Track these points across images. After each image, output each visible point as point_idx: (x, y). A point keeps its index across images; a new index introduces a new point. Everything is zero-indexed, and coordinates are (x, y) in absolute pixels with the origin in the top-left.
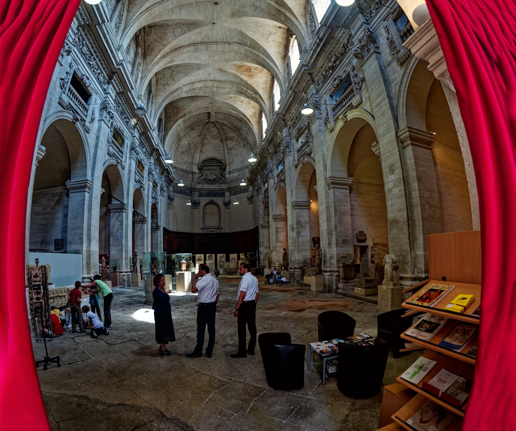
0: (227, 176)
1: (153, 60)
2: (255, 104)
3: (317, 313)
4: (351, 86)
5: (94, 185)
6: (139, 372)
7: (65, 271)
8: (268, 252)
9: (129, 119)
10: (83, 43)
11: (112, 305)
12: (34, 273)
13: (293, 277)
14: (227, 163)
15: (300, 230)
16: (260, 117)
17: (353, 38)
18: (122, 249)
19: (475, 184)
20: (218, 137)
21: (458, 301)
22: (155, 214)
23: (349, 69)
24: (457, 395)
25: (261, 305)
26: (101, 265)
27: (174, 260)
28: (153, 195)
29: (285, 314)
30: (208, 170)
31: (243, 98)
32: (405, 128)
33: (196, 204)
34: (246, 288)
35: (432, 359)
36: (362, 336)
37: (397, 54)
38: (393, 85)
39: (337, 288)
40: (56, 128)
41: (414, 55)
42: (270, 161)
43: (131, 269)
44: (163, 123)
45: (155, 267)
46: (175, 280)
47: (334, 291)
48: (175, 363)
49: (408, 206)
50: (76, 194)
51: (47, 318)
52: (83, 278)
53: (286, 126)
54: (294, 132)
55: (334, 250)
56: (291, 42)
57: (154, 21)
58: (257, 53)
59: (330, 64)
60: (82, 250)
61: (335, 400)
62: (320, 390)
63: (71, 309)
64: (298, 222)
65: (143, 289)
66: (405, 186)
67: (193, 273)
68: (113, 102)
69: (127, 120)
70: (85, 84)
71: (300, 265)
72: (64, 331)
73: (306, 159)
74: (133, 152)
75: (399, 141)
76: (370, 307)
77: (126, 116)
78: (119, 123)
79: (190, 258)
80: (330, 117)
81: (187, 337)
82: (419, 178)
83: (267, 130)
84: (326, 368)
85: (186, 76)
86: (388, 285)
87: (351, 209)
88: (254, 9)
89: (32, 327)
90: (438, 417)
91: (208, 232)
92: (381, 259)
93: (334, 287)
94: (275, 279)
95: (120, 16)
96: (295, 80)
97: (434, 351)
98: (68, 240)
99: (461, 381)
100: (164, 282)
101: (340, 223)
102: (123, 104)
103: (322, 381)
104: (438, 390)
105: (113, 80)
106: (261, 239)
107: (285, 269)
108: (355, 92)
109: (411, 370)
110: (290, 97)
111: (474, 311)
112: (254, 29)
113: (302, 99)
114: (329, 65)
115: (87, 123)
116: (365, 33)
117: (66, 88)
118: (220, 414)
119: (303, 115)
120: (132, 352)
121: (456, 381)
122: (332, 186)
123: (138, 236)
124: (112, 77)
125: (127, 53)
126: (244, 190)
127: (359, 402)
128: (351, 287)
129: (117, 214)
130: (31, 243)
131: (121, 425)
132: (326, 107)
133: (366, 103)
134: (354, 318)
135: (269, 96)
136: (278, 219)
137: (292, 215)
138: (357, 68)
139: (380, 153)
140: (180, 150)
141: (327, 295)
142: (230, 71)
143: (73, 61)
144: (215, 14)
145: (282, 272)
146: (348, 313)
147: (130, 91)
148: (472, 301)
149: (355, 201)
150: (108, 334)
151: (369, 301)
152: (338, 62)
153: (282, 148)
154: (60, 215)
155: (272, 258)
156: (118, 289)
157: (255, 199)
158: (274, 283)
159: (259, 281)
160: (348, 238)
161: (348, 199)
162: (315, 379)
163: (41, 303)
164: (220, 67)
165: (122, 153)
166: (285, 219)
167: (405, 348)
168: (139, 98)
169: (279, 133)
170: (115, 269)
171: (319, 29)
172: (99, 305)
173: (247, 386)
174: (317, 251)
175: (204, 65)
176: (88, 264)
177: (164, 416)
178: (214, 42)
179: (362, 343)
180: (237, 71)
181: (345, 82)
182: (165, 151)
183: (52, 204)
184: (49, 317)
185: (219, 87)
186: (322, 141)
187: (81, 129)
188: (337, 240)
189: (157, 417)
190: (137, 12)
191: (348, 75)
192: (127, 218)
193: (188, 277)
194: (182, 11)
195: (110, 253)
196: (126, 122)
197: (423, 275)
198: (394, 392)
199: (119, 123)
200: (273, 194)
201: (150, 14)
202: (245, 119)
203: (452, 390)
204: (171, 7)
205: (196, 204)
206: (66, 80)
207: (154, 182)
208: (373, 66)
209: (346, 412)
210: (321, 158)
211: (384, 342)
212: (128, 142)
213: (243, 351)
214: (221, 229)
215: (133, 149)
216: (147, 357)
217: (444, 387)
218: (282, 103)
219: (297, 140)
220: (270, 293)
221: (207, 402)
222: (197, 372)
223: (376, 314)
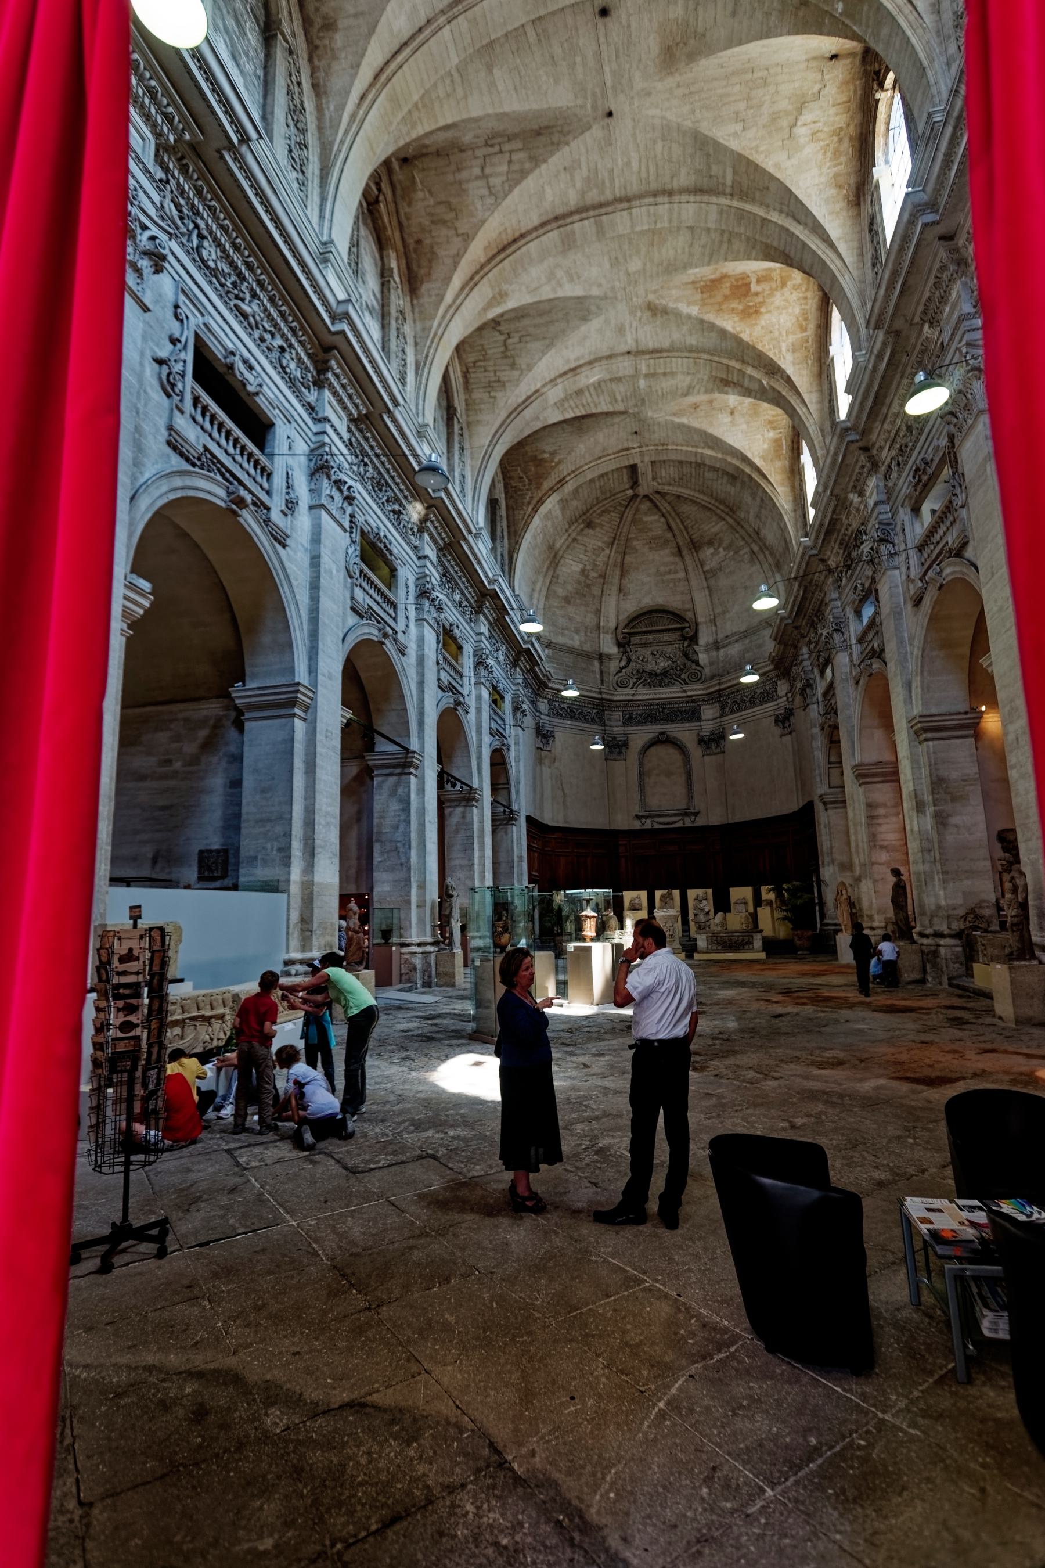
0: (703, 658)
1: (441, 298)
2: (770, 411)
5: (320, 700)
6: (438, 1274)
7: (222, 943)
9: (401, 504)
10: (197, 226)
11: (371, 1044)
12: (120, 948)
14: (700, 620)
16: (796, 452)
18: (408, 881)
20: (666, 542)
22: (503, 780)
26: (344, 923)
27: (560, 910)
28: (494, 725)
29: (877, 1088)
30: (646, 645)
31: (733, 399)
33: (619, 747)
40: (178, 527)
42: (835, 595)
43: (434, 935)
44: (503, 511)
45: (505, 930)
46: (565, 967)
48: (557, 1241)
50: (265, 722)
51: (151, 1086)
52: (288, 963)
53: (875, 466)
54: (904, 483)
56: (882, 108)
57: (414, 135)
58: (761, 212)
60: (288, 881)
63: (239, 1057)
64: (938, 784)
65: (467, 993)
67: (617, 948)
68: (345, 451)
69: (396, 507)
70: (244, 385)
71: (956, 926)
72: (206, 1128)
73: (951, 570)
74: (427, 603)
77: (390, 493)
78: (374, 516)
79: (607, 902)
81: (601, 1151)
85: (549, 347)
89: (87, 1120)
91: (656, 826)
95: (296, 111)
98: (243, 853)
100: (533, 974)
102: (377, 456)
105: (330, 375)
106: (824, 841)
110: (880, 356)
115: (275, 516)
117: (181, 395)
118: (708, 1480)
120: (422, 1197)
123: (456, 842)
124: (326, 362)
125: (356, 272)
129: (392, 780)
130: (114, 860)
131: (340, 1504)
135: (816, 369)
140: (561, 592)
142: (685, 309)
143: (182, 297)
144: (607, 69)
147: (389, 411)
150: (351, 1136)
153: (866, 548)
154: (217, 781)
155: (859, 899)
156: (392, 994)
157: (796, 720)
163: (138, 1039)
164: (651, 297)
165: (394, 606)
166: (892, 774)
168: (420, 435)
169: (855, 498)
170: (386, 934)
172: (333, 1042)
173: (681, 1316)
175: (601, 298)
176: (306, 921)
177: (503, 1465)
178: (620, 200)
180: (703, 303)
182: (517, 597)
183: (190, 748)
184: (158, 1084)
187: (259, 532)
189: (479, 1470)
190: (348, 93)
192: (421, 791)
193: (601, 959)
194: (496, 71)
195: (372, 889)
196: (394, 512)
199: (374, 516)
200: (850, 702)
201: (395, 101)
202: (748, 470)
204: (455, 61)
205: (619, 747)
206: (178, 367)
207: (494, 688)
212: (407, 575)
214: (696, 814)
215: (423, 593)
216: (469, 1217)
219: (916, 510)
220: (845, 1013)
221: (662, 1415)
222: (630, 1281)
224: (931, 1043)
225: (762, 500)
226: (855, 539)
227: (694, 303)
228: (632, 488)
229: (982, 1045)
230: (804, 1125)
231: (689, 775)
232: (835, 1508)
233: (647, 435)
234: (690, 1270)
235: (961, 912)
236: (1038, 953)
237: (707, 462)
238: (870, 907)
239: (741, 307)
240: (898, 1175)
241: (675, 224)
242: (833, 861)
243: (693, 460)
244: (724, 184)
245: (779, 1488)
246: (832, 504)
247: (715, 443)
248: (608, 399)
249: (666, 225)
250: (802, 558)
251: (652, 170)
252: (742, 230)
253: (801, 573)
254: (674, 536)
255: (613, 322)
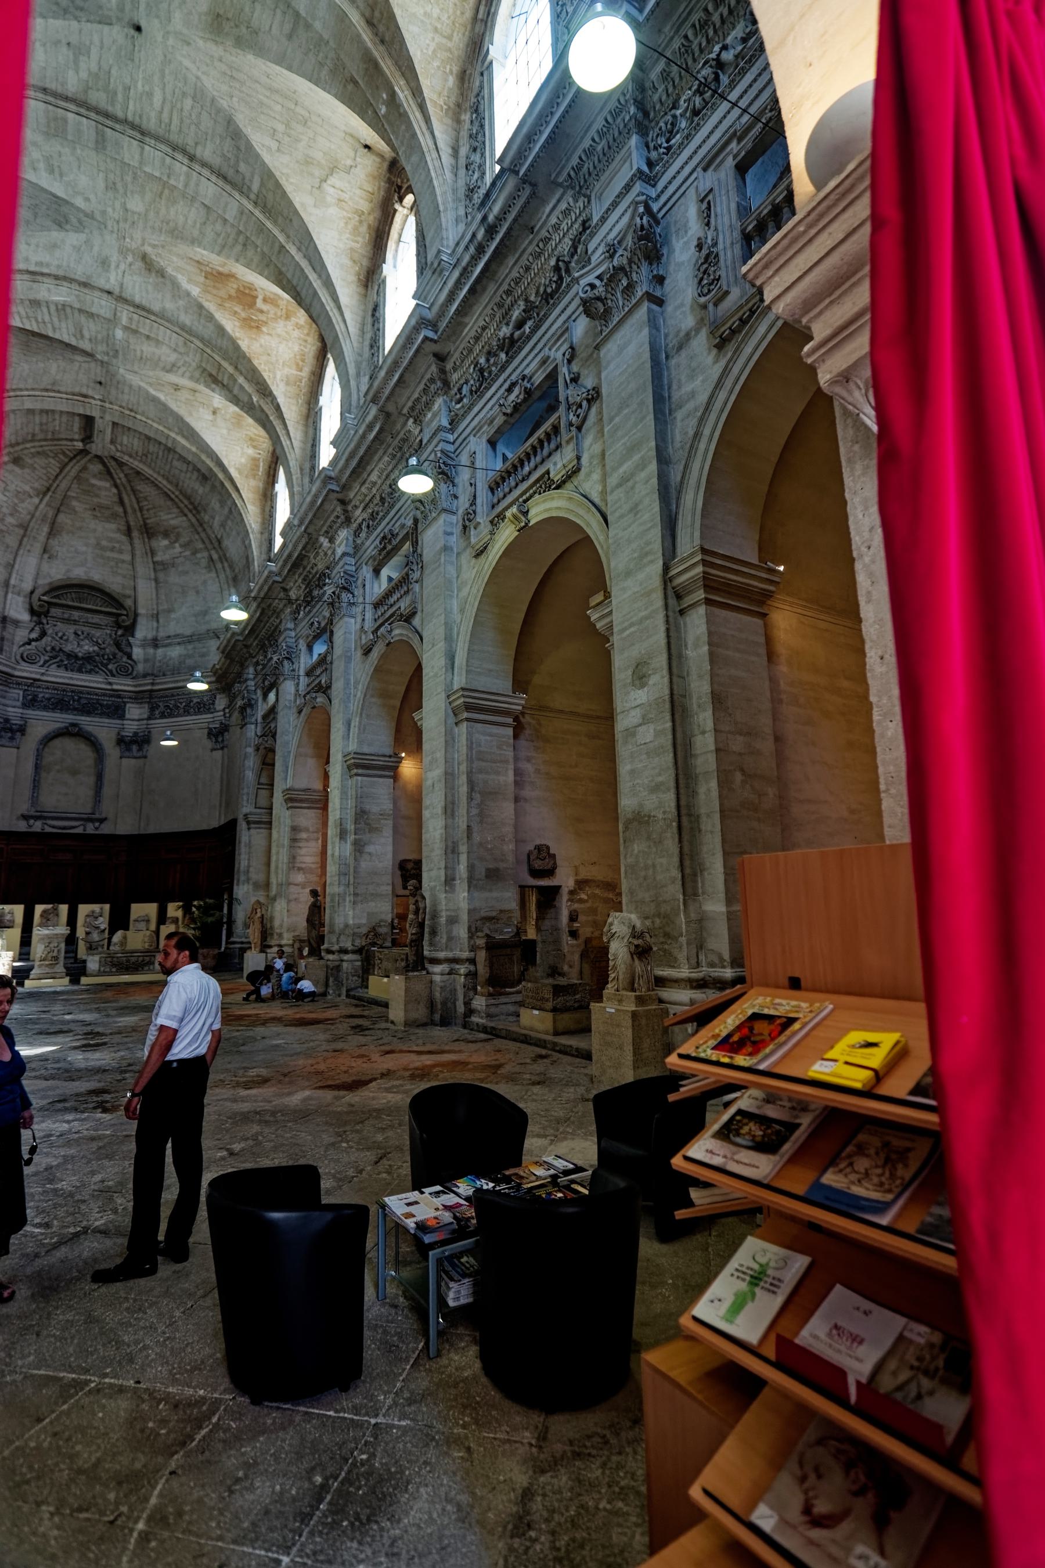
0: (137, 652)
2: (252, 428)
3: (406, 1092)
4: (556, 415)
8: (262, 900)
13: (336, 979)
15: (366, 837)
16: (271, 479)
17: (592, 235)
19: (898, 709)
21: (851, 1053)
23: (557, 354)
24: (919, 1397)
25: (227, 1071)
29: (305, 1100)
31: (218, 400)
32: (692, 554)
34: (179, 1014)
35: (793, 1245)
36: (549, 1166)
37: (716, 305)
38: (679, 415)
39: (470, 1012)
41: (769, 307)
42: (291, 625)
47: (460, 1021)
49: (681, 777)
53: (348, 521)
54: (371, 545)
55: (462, 899)
58: (282, 238)
59: (505, 331)
61: (476, 1422)
62: (423, 1382)
64: (361, 815)
66: (673, 721)
71: (358, 943)
73: (399, 631)
75: (670, 592)
76: (569, 1068)
80: (479, 510)
82: (718, 700)
83: (289, 525)
84: (439, 1287)
86: (620, 1001)
87: (516, 783)
88: (288, 27)
90: (870, 1496)
91: (48, 830)
92: (600, 925)
93: (461, 1008)
94: (280, 986)
96: (390, 373)
97: (793, 1219)
99: (922, 1341)
101: (481, 822)
103: (427, 1344)
104: (841, 1374)
106: (242, 860)
107: (311, 953)
108: (565, 435)
109: (724, 1287)
110: (370, 427)
111: (910, 1084)
112: (281, 128)
113: (404, 440)
114: (501, 334)
116: (632, 218)
119: (403, 493)
121: (901, 1338)
122: (465, 715)
126: (200, 704)
127: (565, 1427)
128: (512, 1008)
132: (473, 476)
133: (588, 475)
134: (521, 1105)
135: (305, 411)
136: (301, 801)
137: (344, 793)
138: (582, 353)
139: (610, 627)
141: (438, 1032)
145: (303, 963)
146: (503, 1089)
148: (900, 1055)
149: (528, 760)
151: (565, 1051)
152: (529, 323)
153: (329, 590)
155: (272, 919)
157: (233, 736)
158: (273, 997)
159: (225, 993)
160: (502, 865)
161: (510, 754)
162: (399, 1335)
164: (148, 249)
166: (322, 803)
167: (690, 1203)
169: (324, 542)
171: (493, 184)
173: (145, 1407)
174: (412, 900)
179: (550, 1189)
180: (206, 291)
181: (541, 398)
185: (135, 332)
186: (450, 582)
188: (471, 868)
191: (552, 377)
197: (728, 973)
198: (681, 1375)
200: (290, 728)
202: (221, 476)
203: (894, 1374)
208: (631, 349)
209: (521, 1479)
210: (441, 631)
211: (622, 1184)
213: (145, 1250)
214: (102, 821)
217: (859, 1360)
218: (343, 445)
219: (377, 572)
220: (260, 1030)
221: (145, 1538)
222: (68, 1389)
223: (588, 1090)
224: (341, 1051)
225: (230, 511)
226: (319, 579)
227: (196, 284)
228: (83, 441)
229: (383, 1048)
230: (243, 1150)
231: (100, 777)
232: (352, 1540)
233: (113, 392)
234: (145, 1348)
235: (364, 930)
236: (427, 965)
237: (178, 450)
238: (281, 926)
239: (243, 315)
240: (340, 1180)
241: (190, 191)
242: (248, 880)
243: (164, 441)
244: (249, 188)
245: (295, 1550)
246: (304, 541)
247: (192, 435)
248: (72, 330)
249: (180, 186)
250: (266, 581)
251: (176, 121)
252: (259, 242)
253: (262, 595)
254: (125, 512)
255: (96, 249)
